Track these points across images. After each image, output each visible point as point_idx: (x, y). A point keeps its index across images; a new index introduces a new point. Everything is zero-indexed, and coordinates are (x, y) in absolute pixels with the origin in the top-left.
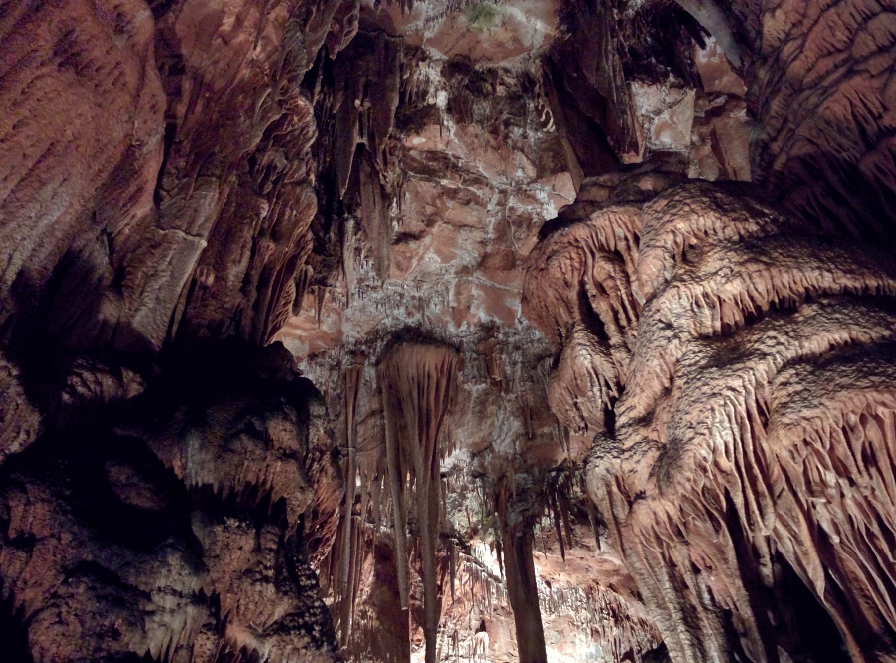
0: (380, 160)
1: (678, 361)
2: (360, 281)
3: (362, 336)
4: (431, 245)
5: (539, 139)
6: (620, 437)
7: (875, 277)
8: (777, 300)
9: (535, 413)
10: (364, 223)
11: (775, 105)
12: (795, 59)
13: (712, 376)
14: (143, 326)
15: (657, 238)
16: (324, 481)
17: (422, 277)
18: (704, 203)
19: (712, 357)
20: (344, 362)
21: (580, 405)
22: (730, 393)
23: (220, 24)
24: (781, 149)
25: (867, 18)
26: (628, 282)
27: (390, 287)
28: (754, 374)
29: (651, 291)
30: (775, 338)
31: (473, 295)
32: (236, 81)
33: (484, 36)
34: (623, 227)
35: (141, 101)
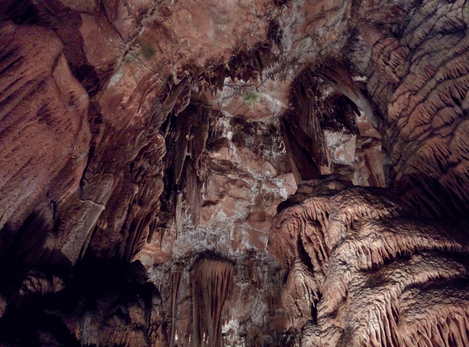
0: (197, 164)
1: (350, 283)
2: (184, 225)
3: (183, 255)
4: (221, 208)
5: (278, 156)
6: (320, 324)
7: (450, 241)
8: (400, 252)
9: (273, 301)
10: (187, 196)
11: (396, 148)
12: (404, 126)
13: (367, 292)
14: (67, 252)
15: (338, 215)
16: (158, 342)
17: (216, 224)
18: (361, 199)
19: (367, 281)
20: (173, 269)
21: (298, 303)
22: (377, 303)
23: (122, 100)
24: (400, 170)
25: (439, 109)
26: (323, 237)
27: (199, 229)
28: (390, 293)
29: (335, 243)
30: (400, 273)
31: (243, 235)
32: (128, 127)
33: (252, 107)
34: (320, 208)
35: (79, 137)
